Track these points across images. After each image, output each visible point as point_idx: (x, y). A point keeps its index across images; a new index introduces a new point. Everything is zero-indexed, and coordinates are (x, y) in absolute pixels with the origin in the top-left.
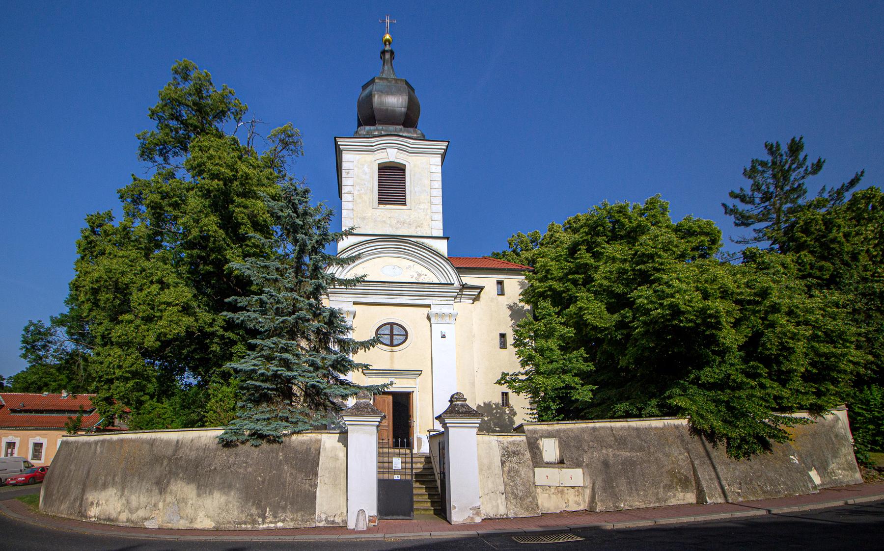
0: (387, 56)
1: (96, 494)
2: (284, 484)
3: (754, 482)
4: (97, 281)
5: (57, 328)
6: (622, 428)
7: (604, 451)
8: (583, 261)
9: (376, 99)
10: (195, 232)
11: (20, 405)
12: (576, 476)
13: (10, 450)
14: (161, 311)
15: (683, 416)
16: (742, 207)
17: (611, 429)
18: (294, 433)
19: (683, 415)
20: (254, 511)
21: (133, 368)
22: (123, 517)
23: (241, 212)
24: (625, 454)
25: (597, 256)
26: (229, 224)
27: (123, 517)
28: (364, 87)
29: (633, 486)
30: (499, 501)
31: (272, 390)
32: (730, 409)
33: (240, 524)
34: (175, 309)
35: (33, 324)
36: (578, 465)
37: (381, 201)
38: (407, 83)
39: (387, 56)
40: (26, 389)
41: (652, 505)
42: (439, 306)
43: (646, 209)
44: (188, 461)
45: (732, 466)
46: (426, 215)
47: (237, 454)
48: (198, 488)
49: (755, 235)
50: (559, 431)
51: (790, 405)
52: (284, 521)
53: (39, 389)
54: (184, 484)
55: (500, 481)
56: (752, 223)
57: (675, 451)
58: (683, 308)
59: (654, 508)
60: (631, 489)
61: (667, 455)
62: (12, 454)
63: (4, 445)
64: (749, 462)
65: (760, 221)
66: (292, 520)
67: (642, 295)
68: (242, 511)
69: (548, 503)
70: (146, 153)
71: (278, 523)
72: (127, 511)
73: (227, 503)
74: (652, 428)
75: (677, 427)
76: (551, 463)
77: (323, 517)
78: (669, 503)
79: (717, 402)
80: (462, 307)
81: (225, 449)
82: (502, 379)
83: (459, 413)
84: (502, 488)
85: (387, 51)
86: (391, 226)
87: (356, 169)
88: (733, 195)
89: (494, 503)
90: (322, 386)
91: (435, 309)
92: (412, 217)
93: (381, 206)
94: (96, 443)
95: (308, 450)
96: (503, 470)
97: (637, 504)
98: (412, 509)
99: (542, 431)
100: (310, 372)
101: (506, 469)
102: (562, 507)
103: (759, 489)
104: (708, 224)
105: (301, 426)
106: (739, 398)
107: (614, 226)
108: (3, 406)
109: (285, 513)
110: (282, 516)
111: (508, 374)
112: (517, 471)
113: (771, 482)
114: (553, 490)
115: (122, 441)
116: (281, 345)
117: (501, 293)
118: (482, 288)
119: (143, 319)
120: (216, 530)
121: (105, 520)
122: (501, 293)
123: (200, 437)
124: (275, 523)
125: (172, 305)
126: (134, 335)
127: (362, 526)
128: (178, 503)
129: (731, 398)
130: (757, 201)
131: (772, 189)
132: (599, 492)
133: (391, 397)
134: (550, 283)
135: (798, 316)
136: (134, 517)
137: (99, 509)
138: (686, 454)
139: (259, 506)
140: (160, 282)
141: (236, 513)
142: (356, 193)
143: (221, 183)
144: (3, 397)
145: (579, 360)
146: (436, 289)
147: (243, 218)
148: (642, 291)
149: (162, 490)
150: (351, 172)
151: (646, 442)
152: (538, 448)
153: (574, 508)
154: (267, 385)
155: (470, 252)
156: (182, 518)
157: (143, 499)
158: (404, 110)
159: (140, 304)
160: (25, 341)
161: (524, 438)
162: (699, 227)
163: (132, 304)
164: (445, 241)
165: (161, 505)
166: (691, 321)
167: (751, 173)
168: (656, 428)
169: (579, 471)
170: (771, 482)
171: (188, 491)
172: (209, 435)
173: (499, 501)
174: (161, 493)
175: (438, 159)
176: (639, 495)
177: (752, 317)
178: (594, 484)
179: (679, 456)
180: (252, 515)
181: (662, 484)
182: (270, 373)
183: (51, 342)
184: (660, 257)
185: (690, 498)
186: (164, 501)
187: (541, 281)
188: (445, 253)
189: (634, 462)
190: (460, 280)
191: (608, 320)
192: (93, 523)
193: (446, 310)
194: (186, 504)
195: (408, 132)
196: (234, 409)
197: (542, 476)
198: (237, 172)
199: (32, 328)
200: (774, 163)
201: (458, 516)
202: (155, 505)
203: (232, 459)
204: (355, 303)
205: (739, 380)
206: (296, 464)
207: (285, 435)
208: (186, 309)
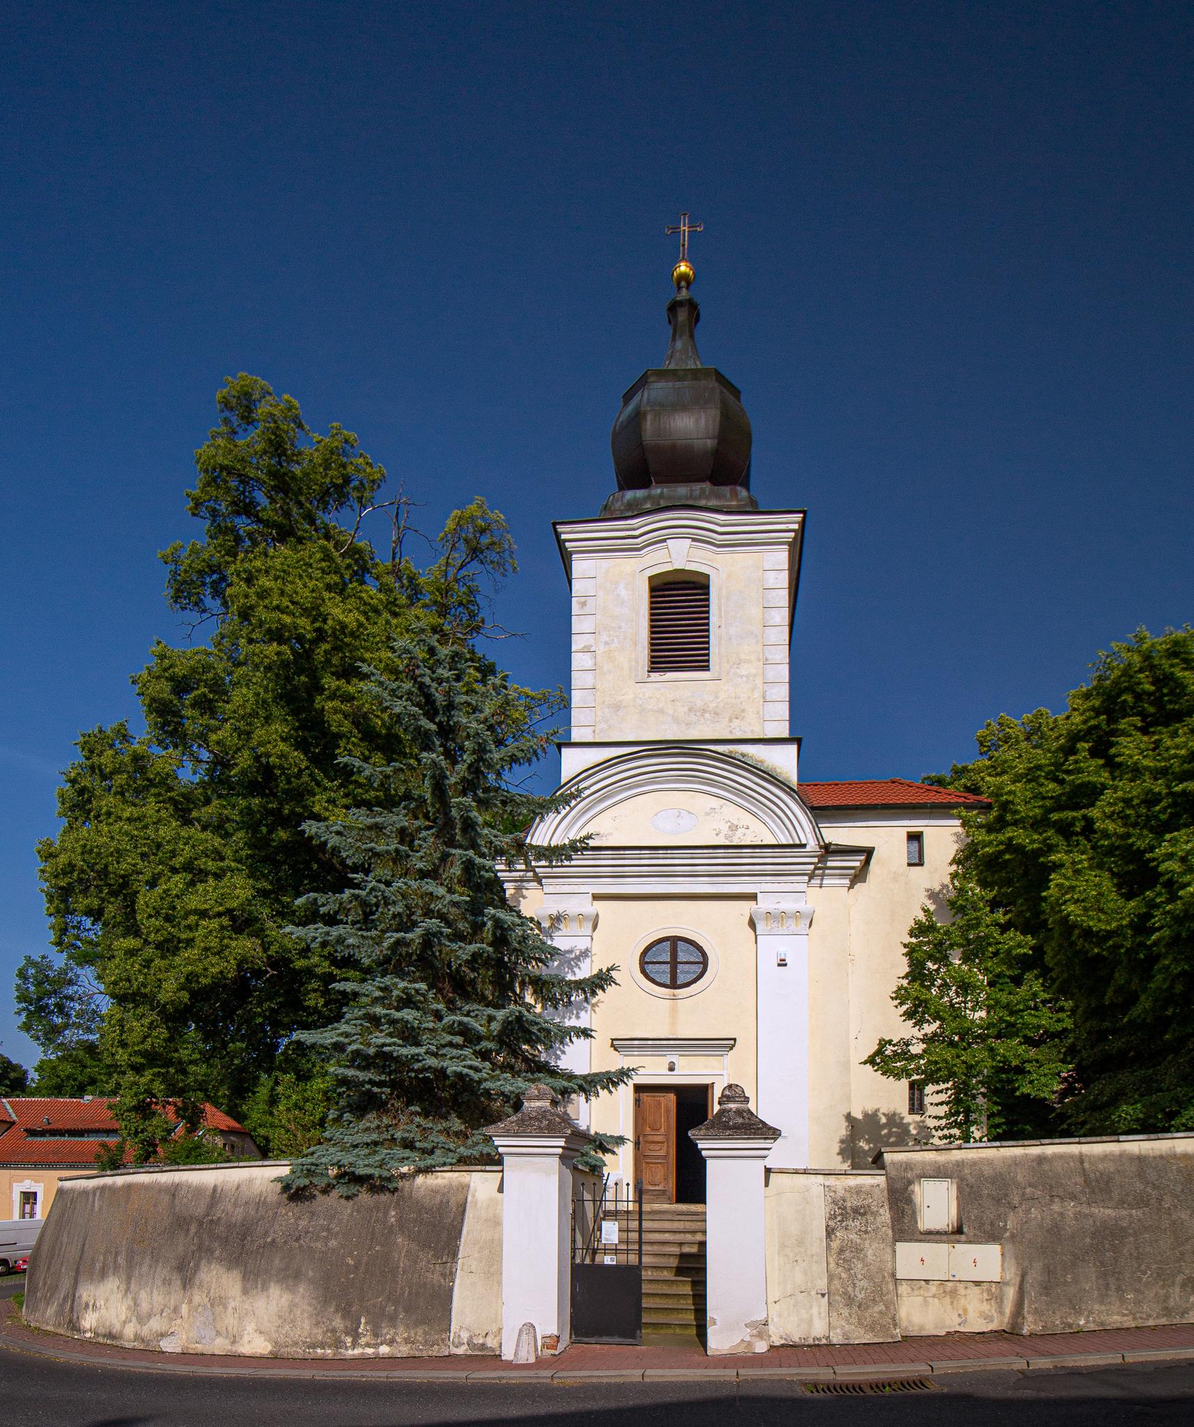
0: (682, 315)
1: (92, 1288)
4: (65, 873)
5: (79, 971)
6: (1105, 1157)
7: (1056, 1207)
8: (1084, 778)
9: (649, 424)
11: (40, 1123)
12: (986, 1260)
13: (28, 1207)
14: (189, 927)
17: (1081, 1159)
18: (419, 1171)
20: (338, 1323)
21: (147, 1046)
22: (130, 1331)
23: (336, 711)
24: (1104, 1212)
26: (316, 739)
27: (130, 1331)
28: (628, 397)
29: (1112, 1280)
30: (815, 1311)
31: (380, 1084)
34: (214, 924)
35: (34, 964)
36: (991, 1235)
38: (720, 378)
39: (682, 315)
40: (58, 1090)
41: (1151, 1323)
42: (776, 896)
44: (230, 1226)
46: (753, 689)
47: (313, 1213)
50: (960, 1164)
52: (391, 1342)
53: (80, 1090)
59: (1154, 1329)
62: (32, 1215)
63: (17, 1198)
66: (407, 1341)
68: (318, 1323)
69: (921, 1315)
70: (185, 592)
71: (379, 1346)
72: (134, 1319)
73: (292, 1306)
76: (938, 1233)
77: (465, 1336)
80: (829, 897)
82: (879, 1052)
84: (822, 1284)
86: (676, 720)
87: (600, 594)
90: (476, 1076)
91: (764, 904)
93: (655, 676)
94: (95, 1190)
95: (444, 1205)
96: (828, 1247)
98: (638, 1325)
99: (924, 1163)
100: (456, 1046)
101: (835, 1245)
105: (439, 1156)
108: (13, 1123)
109: (395, 1327)
110: (388, 1333)
111: (890, 1042)
112: (858, 1250)
114: (933, 1288)
115: (129, 1187)
117: (917, 861)
118: (869, 852)
119: (159, 946)
121: (104, 1336)
122: (917, 861)
123: (251, 1181)
124: (376, 1346)
125: (212, 913)
126: (141, 978)
127: (527, 1356)
128: (212, 1305)
133: (672, 1097)
134: (1010, 833)
136: (145, 1331)
137: (96, 1315)
139: (346, 1314)
140: (188, 867)
142: (601, 649)
144: (13, 1105)
146: (769, 857)
149: (187, 1284)
150: (590, 601)
151: (1155, 1187)
152: (909, 1201)
153: (977, 1324)
154: (370, 1075)
155: (845, 767)
156: (218, 1333)
157: (158, 1298)
158: (710, 443)
159: (150, 916)
160: (22, 998)
161: (881, 1180)
163: (139, 917)
165: (184, 1309)
172: (262, 1177)
173: (815, 1311)
174: (184, 1287)
175: (780, 558)
176: (1122, 1300)
180: (334, 1331)
181: (1179, 1278)
182: (372, 1051)
186: (190, 1301)
187: (990, 829)
188: (793, 778)
189: (1123, 1229)
190: (819, 837)
192: (89, 1342)
193: (788, 904)
194: (225, 1307)
195: (718, 497)
196: (322, 1123)
197: (911, 1259)
198: (325, 621)
201: (719, 1341)
202: (176, 1310)
203: (303, 1223)
204: (596, 897)
206: (419, 1232)
207: (403, 1176)
208: (242, 923)
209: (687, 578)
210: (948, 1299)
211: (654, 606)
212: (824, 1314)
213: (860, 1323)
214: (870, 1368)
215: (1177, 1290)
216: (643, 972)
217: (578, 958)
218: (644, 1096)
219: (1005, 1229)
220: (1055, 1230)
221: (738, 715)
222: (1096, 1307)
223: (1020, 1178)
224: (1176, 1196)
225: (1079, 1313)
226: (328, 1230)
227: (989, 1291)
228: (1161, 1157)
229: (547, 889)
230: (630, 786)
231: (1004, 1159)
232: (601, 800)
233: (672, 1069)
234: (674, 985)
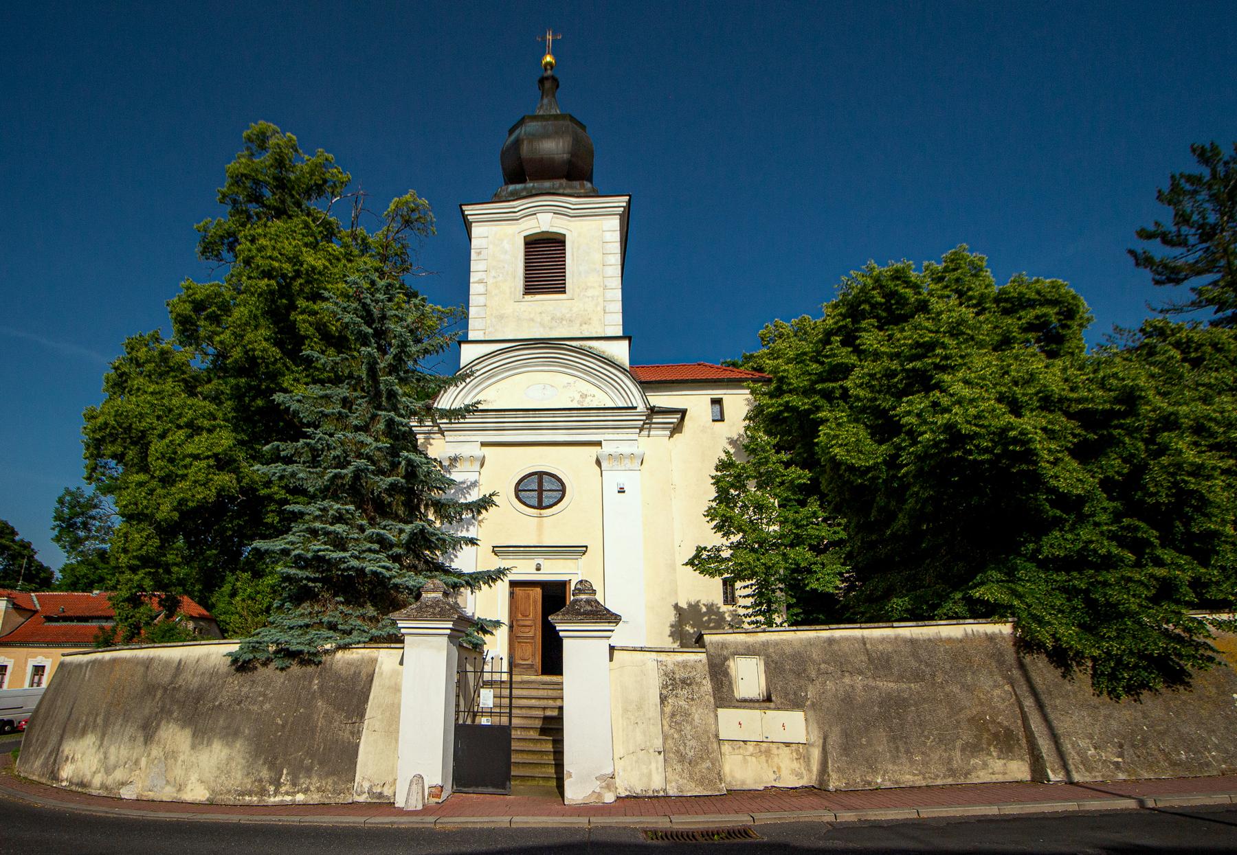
2: (313, 731)
3: (1150, 744)
5: (102, 498)
6: (883, 640)
7: (847, 680)
8: (838, 360)
9: (525, 149)
10: (237, 353)
12: (793, 725)
15: (1002, 618)
16: (1158, 250)
17: (863, 641)
19: (1002, 616)
20: (265, 774)
21: (143, 552)
23: (304, 321)
24: (887, 685)
25: (858, 351)
26: (289, 340)
28: (511, 132)
30: (653, 766)
31: (315, 580)
32: (1091, 604)
33: (243, 794)
34: (203, 464)
36: (795, 703)
37: (530, 289)
39: (548, 84)
41: (939, 782)
42: (615, 442)
43: (946, 270)
45: (1103, 712)
48: (194, 735)
49: (1194, 297)
50: (765, 645)
51: (1221, 596)
52: (306, 791)
53: (89, 587)
54: (177, 729)
56: (1186, 278)
57: (985, 681)
58: (965, 429)
60: (897, 748)
61: (967, 688)
62: (39, 684)
63: (29, 670)
64: (1140, 707)
65: (1199, 273)
66: (319, 790)
67: (910, 408)
69: (743, 771)
71: (297, 794)
73: (230, 759)
74: (941, 640)
75: (991, 638)
76: (751, 701)
77: (366, 785)
78: (974, 779)
79: (1070, 592)
80: (655, 443)
81: (239, 675)
82: (697, 556)
83: (579, 613)
84: (658, 743)
85: (547, 78)
86: (542, 325)
87: (491, 246)
88: (1145, 235)
90: (387, 574)
92: (575, 310)
93: (528, 297)
95: (357, 675)
96: (662, 712)
99: (736, 644)
101: (668, 710)
103: (1161, 757)
104: (1054, 286)
105: (355, 636)
106: (1105, 584)
107: (888, 301)
108: (36, 612)
109: (309, 777)
110: (304, 782)
111: (705, 549)
114: (750, 748)
115: (114, 661)
116: (331, 512)
118: (683, 412)
120: (210, 805)
121: (77, 785)
123: (208, 656)
126: (145, 502)
127: (416, 804)
128: (166, 758)
129: (1092, 584)
130: (1192, 240)
131: (1212, 218)
132: (833, 754)
133: (539, 590)
134: (786, 398)
135: (1212, 435)
136: (109, 781)
137: (73, 767)
138: (1007, 687)
140: (190, 425)
141: (239, 776)
142: (490, 281)
143: (273, 282)
145: (818, 520)
147: (307, 330)
148: (910, 403)
150: (484, 252)
151: (927, 665)
152: (726, 674)
153: (789, 781)
157: (124, 752)
162: (1038, 293)
164: (626, 343)
165: (143, 761)
166: (986, 450)
167: (1173, 196)
168: (950, 640)
171: (175, 736)
172: (215, 653)
173: (653, 766)
175: (614, 223)
176: (912, 762)
177: (1127, 440)
178: (825, 739)
179: (995, 694)
180: (261, 781)
181: (959, 743)
182: (310, 555)
183: (94, 518)
184: (944, 346)
185: (1019, 770)
186: (149, 755)
187: (771, 395)
189: (904, 700)
190: (646, 402)
191: (872, 454)
192: (64, 790)
193: (625, 449)
194: (176, 760)
195: (571, 187)
197: (730, 722)
198: (301, 265)
199: (68, 498)
200: (1214, 175)
201: (575, 792)
202: (137, 762)
204: (483, 444)
205: (1103, 551)
206: (336, 697)
207: (326, 652)
208: (223, 463)
209: (545, 237)
210: (763, 757)
211: (527, 253)
212: (661, 769)
213: (691, 778)
215: (959, 753)
216: (517, 497)
217: (469, 487)
218: (517, 590)
222: (890, 767)
224: (946, 673)
225: (875, 771)
226: (265, 695)
227: (797, 751)
228: (930, 640)
229: (448, 439)
231: (801, 640)
232: (489, 378)
233: (538, 569)
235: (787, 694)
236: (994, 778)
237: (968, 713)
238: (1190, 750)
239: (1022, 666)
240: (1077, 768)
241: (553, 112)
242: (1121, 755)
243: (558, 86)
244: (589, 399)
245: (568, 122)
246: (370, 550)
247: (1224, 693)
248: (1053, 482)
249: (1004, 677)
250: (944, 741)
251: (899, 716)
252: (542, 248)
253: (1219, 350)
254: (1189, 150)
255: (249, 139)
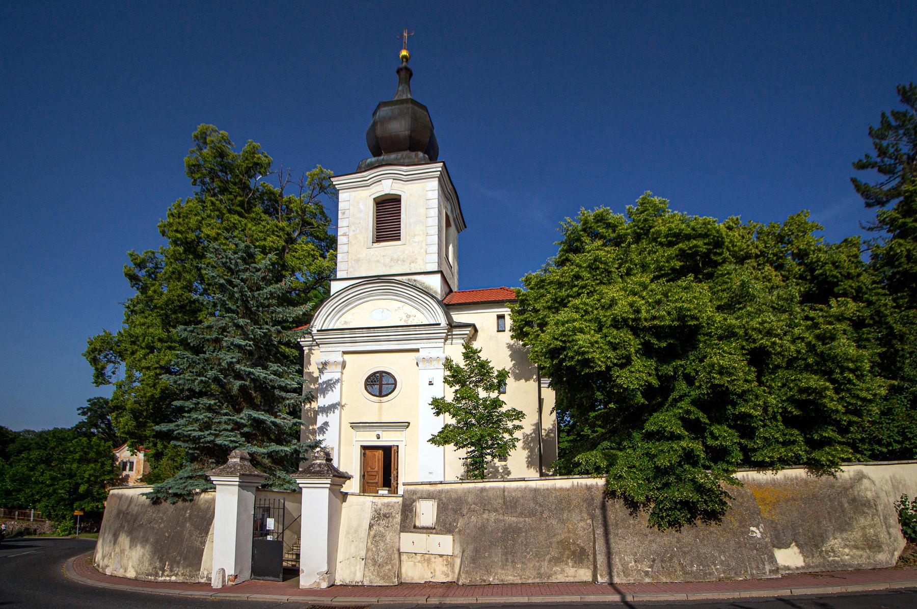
3: (675, 560)
7: (485, 516)
12: (446, 543)
20: (158, 564)
24: (511, 519)
30: (358, 567)
33: (148, 575)
36: (449, 531)
39: (403, 74)
41: (530, 581)
50: (440, 492)
52: (176, 575)
55: (363, 546)
60: (507, 560)
61: (562, 521)
64: (677, 534)
69: (413, 572)
73: (144, 555)
74: (555, 489)
75: (589, 488)
76: (427, 528)
77: (206, 573)
84: (363, 553)
86: (385, 265)
89: (353, 570)
93: (376, 245)
96: (369, 534)
97: (511, 578)
99: (423, 491)
101: (372, 533)
102: (428, 577)
103: (678, 568)
110: (176, 570)
112: (383, 536)
113: (702, 560)
114: (419, 557)
120: (135, 580)
124: (170, 576)
133: (381, 452)
138: (589, 521)
142: (351, 234)
150: (347, 212)
151: (541, 506)
153: (441, 578)
162: (693, 229)
168: (561, 489)
169: (449, 538)
170: (702, 560)
173: (358, 567)
175: (434, 184)
176: (514, 568)
178: (463, 552)
179: (581, 525)
181: (548, 557)
185: (584, 574)
197: (408, 542)
204: (344, 353)
207: (197, 493)
209: (390, 197)
210: (426, 564)
211: (378, 211)
212: (362, 569)
213: (378, 575)
214: (357, 599)
215: (546, 563)
217: (334, 383)
218: (367, 452)
219: (456, 527)
220: (482, 528)
221: (413, 261)
222: (500, 571)
223: (469, 500)
224: (551, 511)
225: (489, 573)
226: (162, 519)
227: (447, 560)
228: (548, 489)
230: (359, 298)
231: (464, 489)
232: (346, 306)
233: (378, 438)
234: (381, 395)
235: (445, 524)
236: (567, 580)
237: (559, 538)
238: (702, 564)
239: (603, 507)
240: (618, 574)
241: (404, 97)
242: (651, 567)
243: (411, 75)
244: (411, 319)
245: (410, 105)
246: (226, 430)
247: (744, 526)
248: (619, 381)
249: (589, 514)
250: (538, 556)
251: (513, 539)
252: (388, 206)
253: (837, 267)
254: (896, 90)
255: (196, 137)
